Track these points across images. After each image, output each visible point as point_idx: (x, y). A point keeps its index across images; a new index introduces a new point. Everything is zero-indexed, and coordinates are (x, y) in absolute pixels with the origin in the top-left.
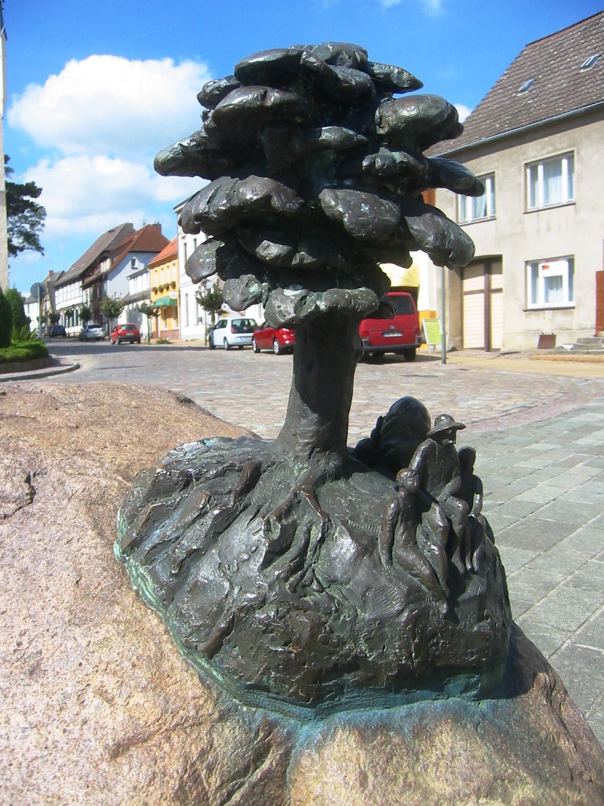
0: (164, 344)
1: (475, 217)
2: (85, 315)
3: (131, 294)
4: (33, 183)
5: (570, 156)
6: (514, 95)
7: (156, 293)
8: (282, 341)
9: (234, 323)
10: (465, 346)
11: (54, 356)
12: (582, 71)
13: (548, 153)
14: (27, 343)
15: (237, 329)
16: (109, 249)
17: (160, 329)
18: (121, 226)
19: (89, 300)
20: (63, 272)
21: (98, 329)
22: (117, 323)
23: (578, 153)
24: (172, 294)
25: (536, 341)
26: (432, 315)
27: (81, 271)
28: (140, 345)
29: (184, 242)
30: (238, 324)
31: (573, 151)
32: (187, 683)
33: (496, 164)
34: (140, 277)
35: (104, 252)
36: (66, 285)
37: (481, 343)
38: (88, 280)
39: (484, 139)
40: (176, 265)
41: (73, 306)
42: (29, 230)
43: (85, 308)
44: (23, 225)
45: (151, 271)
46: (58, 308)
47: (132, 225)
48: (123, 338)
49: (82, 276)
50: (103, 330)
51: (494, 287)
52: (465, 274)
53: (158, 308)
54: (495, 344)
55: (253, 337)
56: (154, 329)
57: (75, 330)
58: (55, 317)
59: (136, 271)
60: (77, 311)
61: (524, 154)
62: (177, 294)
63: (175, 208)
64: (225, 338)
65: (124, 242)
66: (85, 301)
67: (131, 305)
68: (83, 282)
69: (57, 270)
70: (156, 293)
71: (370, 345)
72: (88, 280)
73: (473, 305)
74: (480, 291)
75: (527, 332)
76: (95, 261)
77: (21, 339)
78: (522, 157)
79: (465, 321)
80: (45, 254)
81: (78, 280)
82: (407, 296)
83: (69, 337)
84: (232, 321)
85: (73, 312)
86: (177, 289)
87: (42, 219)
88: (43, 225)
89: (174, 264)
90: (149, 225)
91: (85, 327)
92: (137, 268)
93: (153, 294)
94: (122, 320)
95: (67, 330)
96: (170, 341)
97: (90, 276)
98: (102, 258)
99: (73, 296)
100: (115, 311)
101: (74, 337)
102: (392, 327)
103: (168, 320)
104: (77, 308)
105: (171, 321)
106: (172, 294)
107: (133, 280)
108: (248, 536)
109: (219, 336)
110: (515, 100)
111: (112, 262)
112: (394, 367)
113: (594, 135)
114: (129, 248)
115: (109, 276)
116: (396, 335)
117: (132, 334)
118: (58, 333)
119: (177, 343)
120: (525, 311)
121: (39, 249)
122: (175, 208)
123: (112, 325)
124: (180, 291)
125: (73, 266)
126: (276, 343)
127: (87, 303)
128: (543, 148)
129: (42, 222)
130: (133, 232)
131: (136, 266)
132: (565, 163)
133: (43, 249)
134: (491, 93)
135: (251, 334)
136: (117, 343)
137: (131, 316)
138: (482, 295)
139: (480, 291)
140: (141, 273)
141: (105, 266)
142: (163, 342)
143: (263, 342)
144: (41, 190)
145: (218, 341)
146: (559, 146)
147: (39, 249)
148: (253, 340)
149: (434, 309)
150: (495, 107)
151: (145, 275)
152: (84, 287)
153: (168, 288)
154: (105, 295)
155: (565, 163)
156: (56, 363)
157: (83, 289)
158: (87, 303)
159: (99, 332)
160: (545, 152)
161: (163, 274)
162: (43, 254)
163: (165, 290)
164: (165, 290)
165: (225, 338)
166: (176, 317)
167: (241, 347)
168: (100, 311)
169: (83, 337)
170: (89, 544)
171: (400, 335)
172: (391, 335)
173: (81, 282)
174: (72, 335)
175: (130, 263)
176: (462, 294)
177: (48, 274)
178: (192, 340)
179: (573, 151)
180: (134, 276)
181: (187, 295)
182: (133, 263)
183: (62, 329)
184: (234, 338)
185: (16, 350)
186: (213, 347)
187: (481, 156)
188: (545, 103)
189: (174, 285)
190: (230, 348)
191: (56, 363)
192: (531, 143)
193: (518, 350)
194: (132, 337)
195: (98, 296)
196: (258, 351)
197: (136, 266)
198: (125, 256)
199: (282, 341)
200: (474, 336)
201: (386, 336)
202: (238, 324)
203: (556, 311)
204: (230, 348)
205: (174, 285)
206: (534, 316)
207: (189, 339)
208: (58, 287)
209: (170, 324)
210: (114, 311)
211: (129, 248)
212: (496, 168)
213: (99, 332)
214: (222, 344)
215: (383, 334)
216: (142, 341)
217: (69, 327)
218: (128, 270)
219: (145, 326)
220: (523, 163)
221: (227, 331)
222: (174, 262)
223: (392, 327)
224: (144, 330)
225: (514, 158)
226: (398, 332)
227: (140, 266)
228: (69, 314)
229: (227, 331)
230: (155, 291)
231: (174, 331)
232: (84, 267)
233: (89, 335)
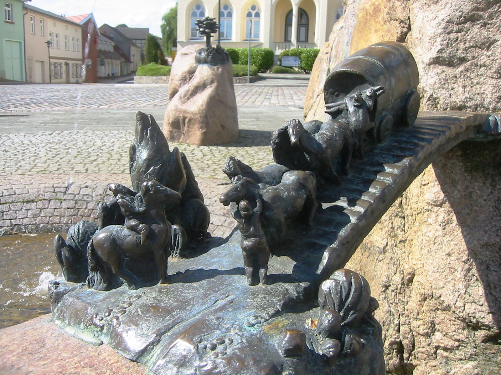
121: (46, 43)
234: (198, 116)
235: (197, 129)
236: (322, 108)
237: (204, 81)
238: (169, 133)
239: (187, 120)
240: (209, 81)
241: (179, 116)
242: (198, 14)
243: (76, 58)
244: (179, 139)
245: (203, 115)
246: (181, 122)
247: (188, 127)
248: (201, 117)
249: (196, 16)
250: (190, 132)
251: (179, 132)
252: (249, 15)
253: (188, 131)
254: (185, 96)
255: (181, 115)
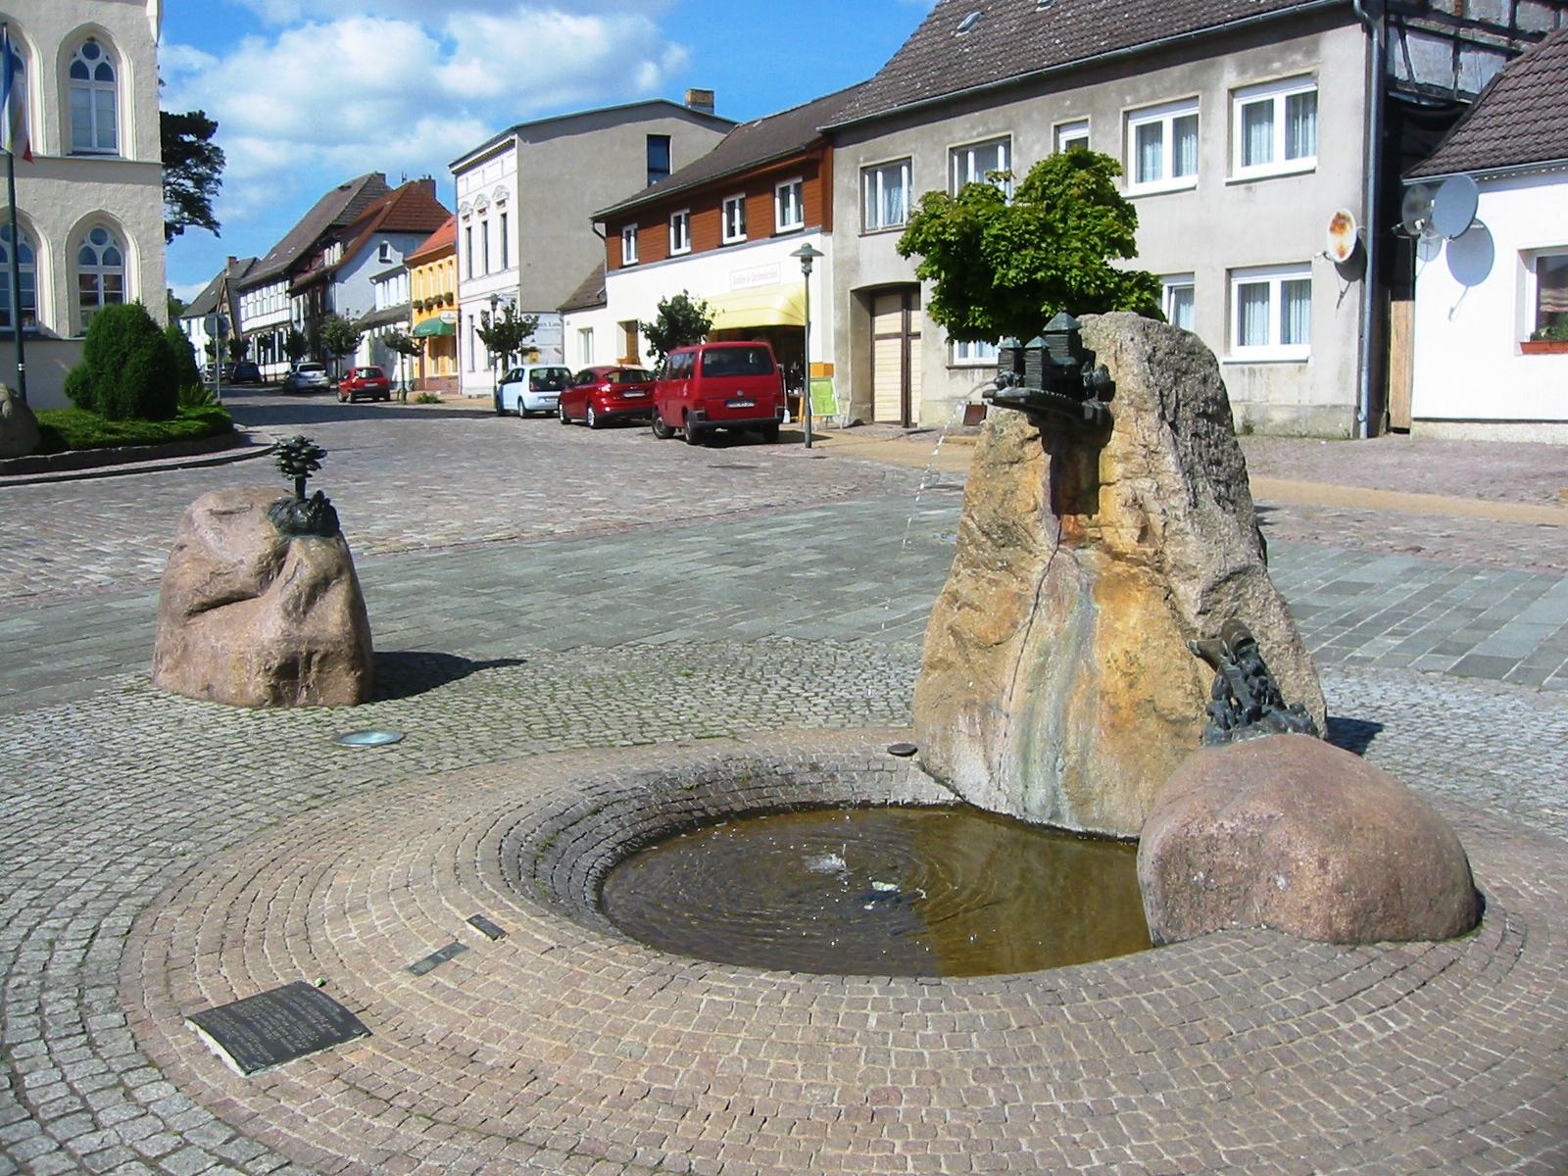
0: (429, 407)
1: (889, 222)
2: (295, 347)
3: (379, 308)
4: (202, 114)
5: (1006, 141)
6: (952, 33)
7: (420, 311)
8: (599, 408)
9: (534, 375)
10: (876, 419)
11: (239, 427)
12: (1039, 9)
13: (979, 135)
14: (200, 411)
15: (538, 385)
16: (346, 221)
17: (427, 375)
18: (362, 178)
19: (302, 316)
20: (255, 259)
21: (318, 373)
22: (353, 362)
23: (1016, 139)
24: (446, 315)
25: (961, 410)
26: (828, 370)
27: (287, 262)
28: (388, 405)
29: (468, 225)
30: (543, 375)
31: (1009, 136)
32: (275, 531)
33: (913, 146)
34: (393, 281)
35: (331, 228)
36: (260, 288)
37: (896, 414)
38: (301, 279)
39: (896, 108)
40: (455, 263)
41: (275, 326)
42: (192, 190)
43: (294, 332)
44: (181, 181)
45: (412, 271)
46: (245, 327)
47: (383, 176)
48: (359, 392)
49: (289, 273)
50: (326, 375)
51: (914, 329)
52: (878, 306)
53: (422, 339)
54: (915, 417)
55: (560, 399)
56: (417, 375)
57: (277, 369)
58: (240, 347)
59: (388, 267)
60: (281, 334)
61: (949, 133)
62: (455, 314)
63: (451, 166)
64: (520, 399)
65: (365, 214)
66: (295, 318)
67: (376, 330)
68: (291, 284)
69: (244, 256)
70: (420, 311)
71: (707, 419)
72: (301, 279)
73: (888, 354)
74: (896, 336)
75: (951, 400)
76: (314, 245)
77: (191, 404)
78: (947, 139)
79: (877, 380)
80: (296, 719)
81: (283, 280)
82: (765, 348)
83: (267, 384)
84: (531, 371)
85: (273, 336)
86: (456, 307)
87: (216, 171)
88: (219, 182)
89: (451, 263)
90: (413, 182)
91: (294, 367)
92: (389, 262)
93: (415, 311)
94: (362, 358)
95: (261, 370)
96: (439, 398)
97: (305, 273)
98: (326, 240)
99: (270, 309)
100: (347, 342)
101: (276, 383)
102: (740, 393)
103: (439, 359)
104: (281, 330)
105: (446, 361)
106: (446, 315)
107: (381, 284)
108: (286, 510)
109: (512, 394)
110: (953, 43)
111: (345, 249)
112: (737, 453)
113: (1035, 115)
114: (376, 223)
115: (339, 276)
116: (745, 405)
117: (376, 384)
118: (245, 376)
119: (452, 401)
120: (949, 368)
121: (211, 224)
122: (451, 166)
123: (344, 363)
124: (459, 310)
125: (273, 251)
126: (590, 410)
127: (298, 321)
128: (973, 127)
129: (216, 176)
130: (384, 190)
131: (388, 257)
132: (1001, 150)
133: (218, 224)
134: (925, 24)
135: (558, 393)
136: (349, 399)
137: (375, 354)
138: (899, 341)
139: (896, 336)
140: (395, 273)
141: (333, 255)
142: (428, 400)
143: (573, 407)
144: (216, 124)
145: (510, 403)
146: (992, 127)
147: (211, 224)
148: (559, 403)
149: (831, 360)
150: (925, 50)
151: (402, 277)
152: (293, 293)
153: (440, 305)
154: (332, 311)
155: (1001, 150)
156: (243, 440)
157: (293, 296)
158: (298, 321)
159: (319, 377)
160: (975, 133)
161: (442, 275)
162: (217, 235)
163: (435, 306)
164: (435, 306)
165: (520, 399)
166: (454, 356)
167: (549, 414)
168: (323, 338)
169: (290, 386)
170: (262, 514)
171: (751, 405)
172: (739, 405)
173: (287, 282)
174: (271, 379)
175: (378, 250)
176: (872, 338)
177: (226, 263)
178: (479, 396)
179: (1009, 136)
180: (383, 278)
181: (471, 317)
182: (383, 252)
183: (254, 367)
184: (533, 399)
185: (185, 423)
186: (502, 412)
187: (909, 128)
188: (983, 57)
189: (450, 299)
190: (530, 414)
191: (243, 440)
192: (957, 119)
193: (932, 427)
194: (379, 385)
195: (319, 310)
196: (567, 422)
197: (388, 257)
198: (369, 238)
199: (599, 408)
200: (888, 407)
201: (731, 406)
202: (543, 375)
203: (987, 370)
204: (530, 414)
205: (450, 299)
206: (959, 377)
207: (474, 393)
208: (245, 291)
209: (443, 366)
210: (346, 342)
211: (376, 223)
212: (914, 151)
213: (319, 377)
214: (516, 408)
215: (726, 403)
216: (393, 396)
217: (265, 364)
218: (372, 265)
219: (402, 370)
220: (948, 147)
221: (523, 388)
222: (450, 258)
223: (740, 393)
224: (397, 374)
225: (936, 139)
226: (749, 401)
227: (395, 257)
228: (266, 343)
229: (523, 388)
230: (419, 307)
231: (450, 378)
232: (293, 253)
233: (302, 383)
234: (344, 647)
235: (343, 673)
236: (921, 420)
237: (325, 571)
238: (269, 689)
239: (316, 658)
240: (334, 570)
241: (296, 652)
242: (86, 61)
243: (604, 107)
244: (295, 698)
245: (352, 643)
246: (301, 662)
247: (319, 671)
248: (350, 646)
249: (86, 76)
250: (325, 680)
251: (292, 685)
252: (78, 71)
253: (319, 680)
254: (296, 608)
255: (303, 649)
